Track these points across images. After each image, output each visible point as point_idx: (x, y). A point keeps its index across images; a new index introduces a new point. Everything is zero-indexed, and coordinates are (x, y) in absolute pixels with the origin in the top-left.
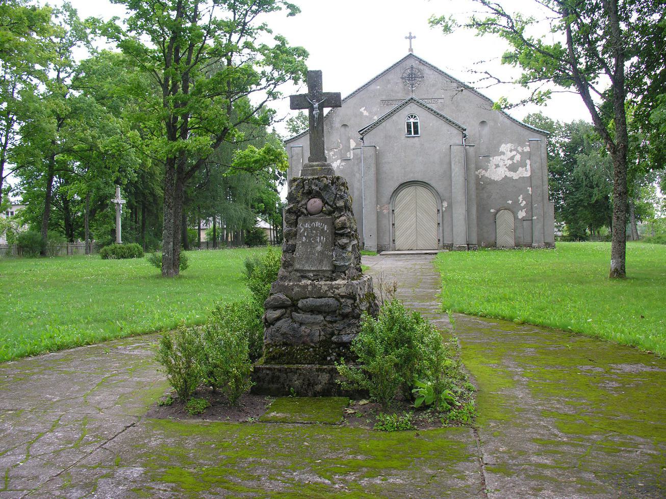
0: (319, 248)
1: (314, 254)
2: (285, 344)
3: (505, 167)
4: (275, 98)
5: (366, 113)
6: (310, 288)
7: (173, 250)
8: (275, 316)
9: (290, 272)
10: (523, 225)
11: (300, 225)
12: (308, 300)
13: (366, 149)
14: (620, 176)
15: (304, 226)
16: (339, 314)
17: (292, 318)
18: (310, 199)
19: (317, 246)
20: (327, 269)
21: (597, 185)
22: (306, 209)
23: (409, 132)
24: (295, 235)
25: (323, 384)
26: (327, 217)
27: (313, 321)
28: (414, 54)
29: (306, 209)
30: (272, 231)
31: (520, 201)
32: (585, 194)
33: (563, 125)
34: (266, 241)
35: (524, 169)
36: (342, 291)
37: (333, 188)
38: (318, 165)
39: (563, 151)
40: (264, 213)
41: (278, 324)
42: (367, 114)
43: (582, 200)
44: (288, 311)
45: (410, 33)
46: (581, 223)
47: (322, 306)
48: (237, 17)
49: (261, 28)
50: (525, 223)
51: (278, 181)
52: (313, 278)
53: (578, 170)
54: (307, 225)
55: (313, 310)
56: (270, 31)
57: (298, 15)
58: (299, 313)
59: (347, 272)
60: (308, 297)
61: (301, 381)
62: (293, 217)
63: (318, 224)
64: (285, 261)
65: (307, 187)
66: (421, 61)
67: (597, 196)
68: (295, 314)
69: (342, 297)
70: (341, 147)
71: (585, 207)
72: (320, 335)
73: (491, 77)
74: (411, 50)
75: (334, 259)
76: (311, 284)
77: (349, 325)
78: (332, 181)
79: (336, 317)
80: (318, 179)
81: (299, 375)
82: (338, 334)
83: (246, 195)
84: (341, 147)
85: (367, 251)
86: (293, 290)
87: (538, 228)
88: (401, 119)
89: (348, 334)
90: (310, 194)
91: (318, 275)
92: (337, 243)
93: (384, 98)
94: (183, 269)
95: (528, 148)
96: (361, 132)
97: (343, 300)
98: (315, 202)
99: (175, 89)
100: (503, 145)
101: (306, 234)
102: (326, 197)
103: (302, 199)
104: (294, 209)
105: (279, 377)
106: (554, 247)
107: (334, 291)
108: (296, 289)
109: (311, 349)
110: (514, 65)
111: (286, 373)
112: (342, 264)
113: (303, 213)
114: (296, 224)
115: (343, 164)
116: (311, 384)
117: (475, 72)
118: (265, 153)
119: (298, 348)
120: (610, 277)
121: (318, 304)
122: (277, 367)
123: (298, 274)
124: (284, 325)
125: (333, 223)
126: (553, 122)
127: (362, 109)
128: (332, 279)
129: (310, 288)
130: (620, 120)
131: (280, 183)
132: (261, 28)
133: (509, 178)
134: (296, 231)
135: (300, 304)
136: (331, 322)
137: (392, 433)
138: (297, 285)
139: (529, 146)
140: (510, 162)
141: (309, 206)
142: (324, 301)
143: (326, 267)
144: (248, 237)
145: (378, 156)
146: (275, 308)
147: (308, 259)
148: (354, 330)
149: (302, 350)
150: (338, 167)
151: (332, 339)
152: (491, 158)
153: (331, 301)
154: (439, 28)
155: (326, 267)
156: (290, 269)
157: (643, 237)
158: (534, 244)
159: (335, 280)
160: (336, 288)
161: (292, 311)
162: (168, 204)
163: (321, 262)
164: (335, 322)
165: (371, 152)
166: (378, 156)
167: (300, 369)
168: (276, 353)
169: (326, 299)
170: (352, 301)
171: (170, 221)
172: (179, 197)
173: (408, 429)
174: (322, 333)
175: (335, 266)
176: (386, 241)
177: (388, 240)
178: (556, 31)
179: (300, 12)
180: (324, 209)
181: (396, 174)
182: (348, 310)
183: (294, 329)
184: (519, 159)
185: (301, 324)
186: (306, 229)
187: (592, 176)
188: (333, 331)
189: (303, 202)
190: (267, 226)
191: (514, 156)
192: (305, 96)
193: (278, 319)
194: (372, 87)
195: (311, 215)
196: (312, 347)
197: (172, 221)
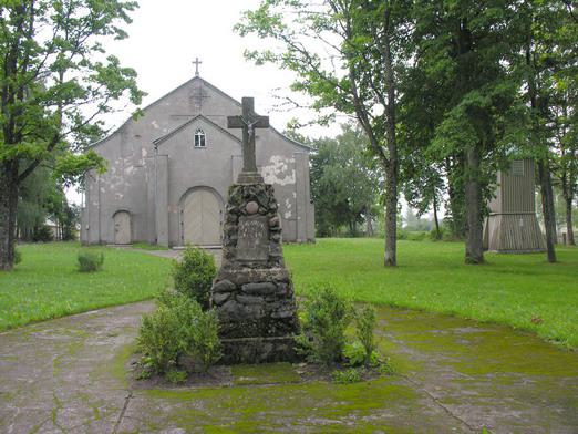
0: (257, 242)
4: (106, 111)
11: (241, 223)
15: (243, 224)
21: (340, 191)
23: (197, 144)
28: (201, 76)
36: (279, 276)
37: (267, 193)
40: (51, 211)
41: (226, 305)
46: (327, 222)
49: (95, 48)
55: (255, 293)
56: (103, 51)
57: (126, 39)
62: (235, 217)
66: (206, 84)
67: (339, 199)
68: (238, 296)
74: (197, 73)
88: (191, 132)
90: (248, 198)
91: (257, 264)
99: (12, 100)
108: (239, 276)
116: (258, 353)
124: (230, 306)
132: (95, 48)
135: (244, 288)
136: (270, 302)
142: (264, 285)
145: (170, 164)
146: (222, 292)
147: (248, 251)
153: (270, 285)
154: (253, 61)
155: (263, 257)
163: (259, 253)
166: (170, 164)
175: (270, 257)
176: (176, 237)
182: (283, 292)
183: (239, 309)
185: (245, 305)
190: (54, 224)
193: (225, 301)
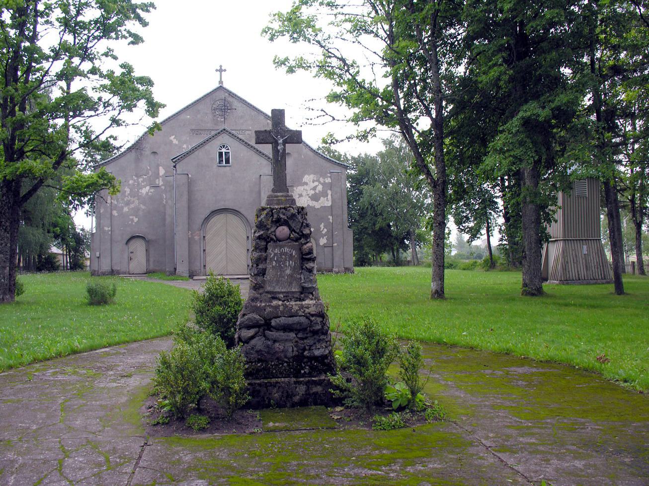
0: (288, 272)
1: (283, 277)
2: (259, 360)
3: (307, 197)
4: (119, 125)
5: (175, 142)
6: (281, 308)
7: (9, 275)
8: (250, 335)
9: (261, 294)
10: (324, 252)
11: (270, 250)
12: (280, 319)
13: (179, 177)
14: (439, 207)
15: (273, 251)
16: (310, 331)
17: (265, 336)
18: (277, 227)
19: (286, 270)
20: (297, 290)
21: (381, 214)
22: (275, 235)
23: (221, 161)
24: (266, 259)
25: (301, 395)
26: (295, 243)
27: (286, 338)
28: (225, 85)
29: (275, 235)
30: (65, 257)
31: (322, 229)
32: (370, 223)
33: (350, 158)
34: (58, 266)
35: (326, 198)
36: (312, 310)
37: (299, 217)
38: (282, 196)
39: (350, 182)
40: (56, 237)
41: (253, 342)
42: (177, 143)
43: (366, 228)
44: (261, 330)
45: (221, 66)
46: (367, 249)
47: (294, 324)
48: (77, 41)
50: (326, 249)
51: (72, 206)
52: (283, 299)
53: (364, 200)
54: (276, 251)
55: (286, 328)
56: (115, 58)
58: (272, 331)
59: (314, 293)
60: (280, 317)
61: (280, 393)
62: (263, 243)
63: (286, 250)
64: (256, 284)
65: (275, 216)
68: (268, 332)
69: (313, 315)
70: (150, 173)
71: (369, 234)
72: (293, 351)
73: (327, 114)
74: (221, 82)
75: (302, 281)
76: (282, 305)
77: (319, 341)
78: (298, 210)
79: (307, 334)
80: (284, 208)
81: (279, 388)
82: (310, 349)
83: (42, 219)
84: (150, 173)
85: (180, 276)
86: (265, 310)
87: (338, 254)
88: (213, 149)
89: (319, 349)
90: (278, 222)
91: (288, 297)
92: (304, 267)
93: (193, 127)
94: (18, 294)
95: (329, 179)
96: (174, 160)
97: (313, 319)
98: (283, 229)
100: (306, 176)
101: (275, 259)
102: (293, 225)
103: (272, 226)
104: (264, 236)
105: (259, 391)
106: (353, 272)
107: (305, 311)
108: (268, 309)
109: (285, 364)
110: (341, 104)
111: (266, 387)
112: (310, 285)
113: (272, 239)
114: (266, 249)
115: (152, 190)
116: (289, 396)
117: (313, 110)
118: (99, 177)
119: (273, 363)
120: (432, 298)
121: (290, 323)
122: (258, 382)
123: (270, 296)
125: (300, 249)
126: (341, 155)
127: (172, 138)
128: (301, 300)
129: (281, 308)
130: (439, 158)
131: (74, 207)
133: (311, 207)
134: (266, 256)
135: (273, 323)
137: (390, 431)
138: (269, 306)
139: (331, 177)
140: (312, 192)
141: (278, 233)
142: (296, 319)
143: (295, 289)
144: (40, 261)
146: (249, 327)
148: (323, 345)
149: (277, 365)
150: (147, 193)
151: (305, 354)
152: (295, 188)
153: (303, 320)
154: (284, 69)
155: (295, 289)
156: (261, 291)
157: (423, 263)
158: (334, 269)
159: (304, 300)
160: (305, 308)
161: (264, 330)
162: (4, 228)
163: (291, 283)
164: (306, 338)
165: (184, 179)
166: (190, 184)
167: (279, 383)
168: (253, 369)
169: (298, 317)
170: (321, 319)
171: (6, 245)
172: (15, 221)
173: (402, 427)
174: (295, 349)
175: (303, 288)
176: (197, 266)
177: (198, 264)
178: (388, 77)
179: (143, 41)
180: (292, 236)
181: (208, 201)
182: (319, 327)
183: (268, 347)
184: (321, 190)
185: (275, 341)
186: (275, 254)
187: (377, 206)
188: (305, 347)
189: (272, 230)
190: (60, 252)
191: (316, 186)
192: (270, 132)
193: (252, 337)
194: (182, 117)
195: (280, 241)
196: (286, 362)
197: (9, 245)
